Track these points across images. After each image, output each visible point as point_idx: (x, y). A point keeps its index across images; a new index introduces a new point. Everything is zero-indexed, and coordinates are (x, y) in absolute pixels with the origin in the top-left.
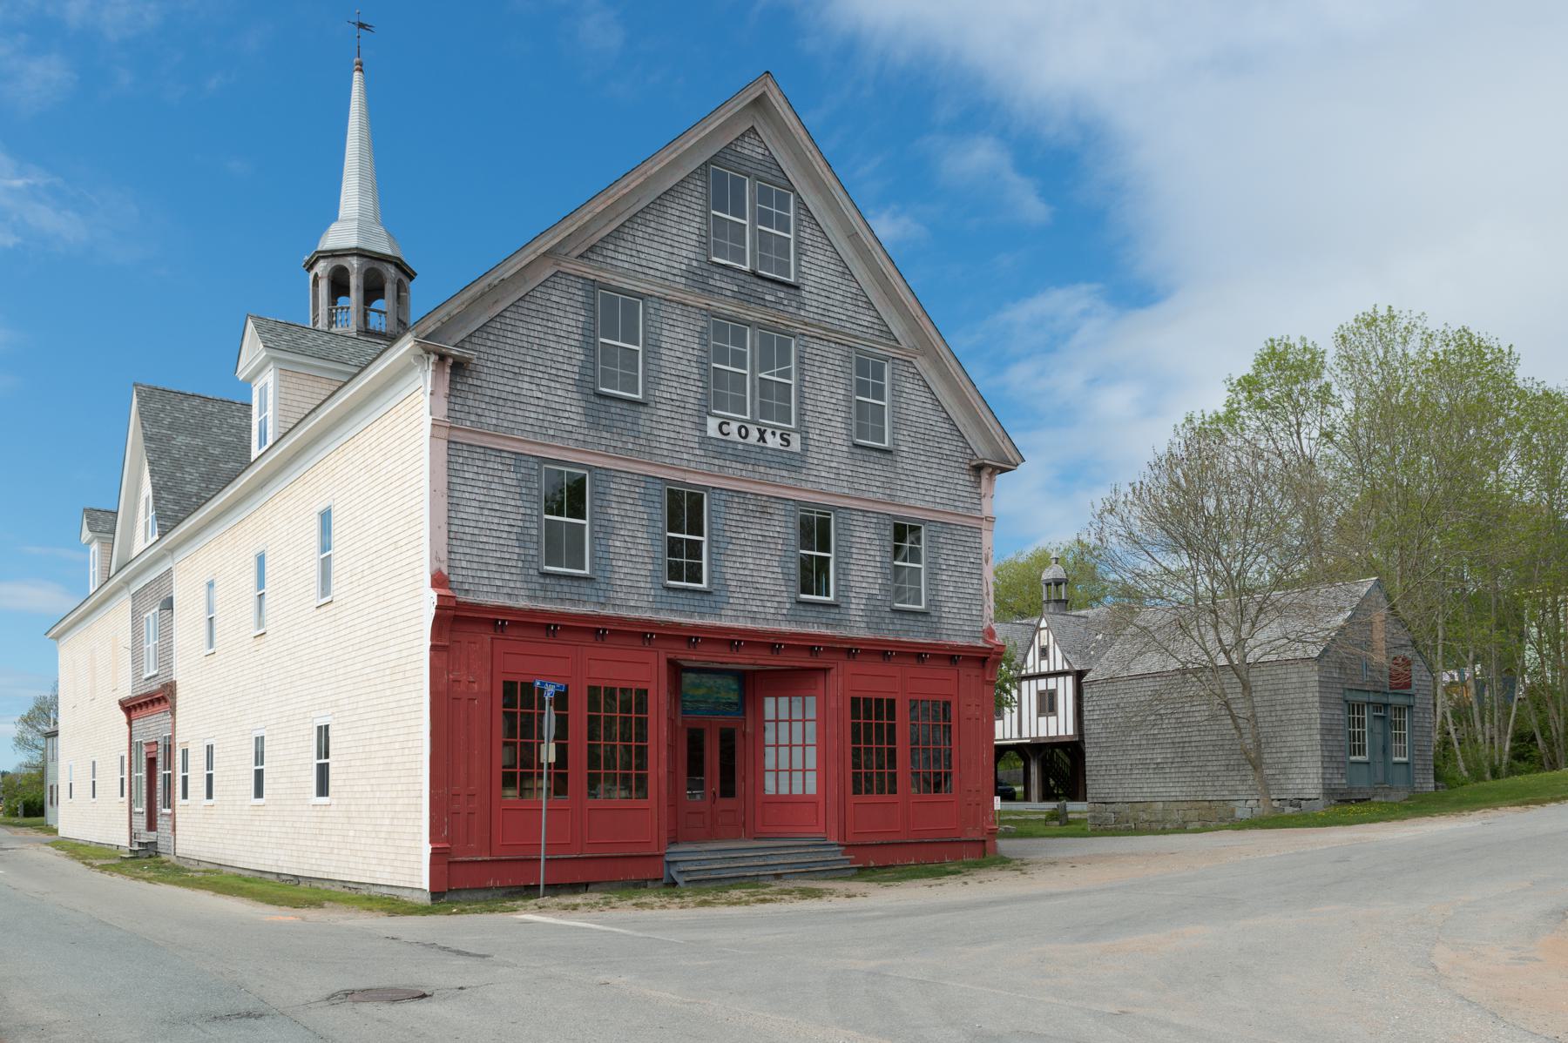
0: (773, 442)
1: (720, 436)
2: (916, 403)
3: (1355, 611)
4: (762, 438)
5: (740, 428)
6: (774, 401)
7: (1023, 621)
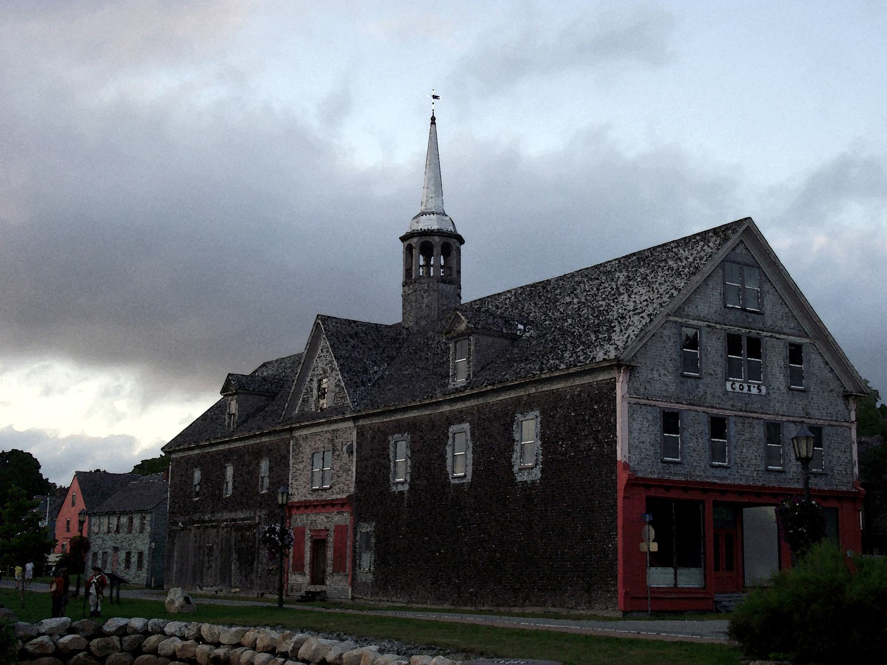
0: (754, 391)
1: (732, 390)
2: (817, 361)
3: (288, 485)
4: (749, 390)
5: (740, 385)
6: (755, 373)
7: (701, 509)
